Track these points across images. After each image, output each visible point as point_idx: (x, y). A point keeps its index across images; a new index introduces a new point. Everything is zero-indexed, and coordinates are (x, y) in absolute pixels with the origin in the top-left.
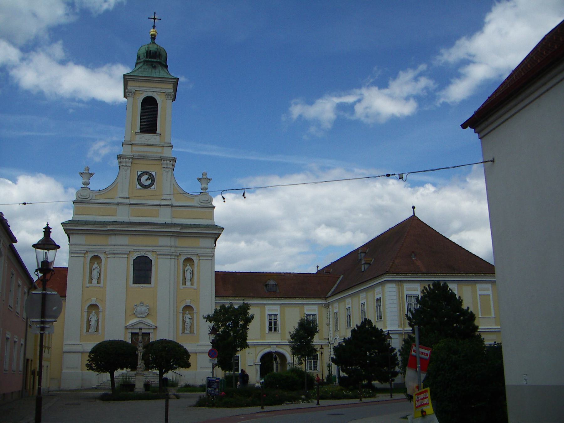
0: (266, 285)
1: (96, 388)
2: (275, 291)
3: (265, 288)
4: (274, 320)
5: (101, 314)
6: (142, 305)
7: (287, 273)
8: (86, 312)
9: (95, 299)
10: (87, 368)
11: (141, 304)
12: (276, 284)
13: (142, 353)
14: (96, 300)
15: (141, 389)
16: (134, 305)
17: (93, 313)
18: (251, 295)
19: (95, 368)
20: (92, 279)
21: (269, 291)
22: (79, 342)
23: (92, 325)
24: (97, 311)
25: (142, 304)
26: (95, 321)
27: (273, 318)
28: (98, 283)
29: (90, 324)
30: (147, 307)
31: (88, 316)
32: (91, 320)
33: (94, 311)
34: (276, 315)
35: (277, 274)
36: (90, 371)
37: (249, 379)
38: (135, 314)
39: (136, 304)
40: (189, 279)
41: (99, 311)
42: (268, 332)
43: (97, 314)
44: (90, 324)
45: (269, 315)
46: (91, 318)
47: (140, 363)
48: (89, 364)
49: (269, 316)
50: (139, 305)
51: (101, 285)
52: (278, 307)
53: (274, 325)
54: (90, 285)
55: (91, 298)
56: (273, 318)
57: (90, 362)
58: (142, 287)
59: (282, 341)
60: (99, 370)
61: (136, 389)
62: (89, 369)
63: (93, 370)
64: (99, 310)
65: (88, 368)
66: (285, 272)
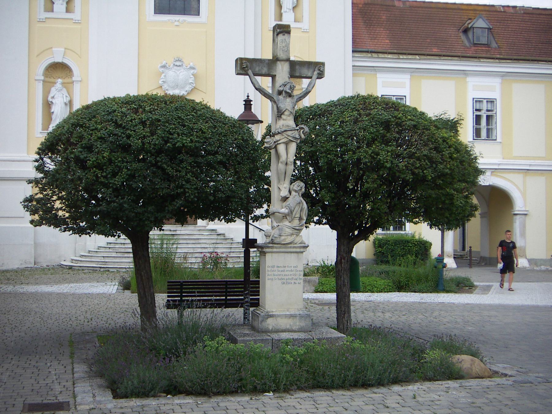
0: (466, 31)
1: (70, 268)
2: (488, 45)
3: (463, 37)
4: (488, 111)
5: (77, 88)
6: (180, 66)
7: (508, 6)
8: (42, 82)
9: (63, 49)
10: (28, 217)
11: (178, 63)
12: (491, 27)
13: (293, 147)
14: (65, 52)
15: (292, 316)
16: (160, 65)
17: (58, 85)
18: (435, 50)
19: (67, 215)
20: (53, 3)
21: (475, 45)
22: (26, 155)
23: (57, 115)
24: (67, 80)
25: (179, 63)
26: (63, 105)
27: (484, 106)
28: (68, 11)
29: (52, 111)
30: (192, 71)
31: (46, 92)
32: (54, 101)
33: (60, 81)
34: (491, 101)
35: (486, 7)
36: (44, 229)
37: (432, 249)
38: (161, 87)
39: (164, 63)
40: (291, 7)
41: (74, 79)
42: (474, 139)
43: (67, 87)
44: (52, 111)
45: (478, 101)
46: (53, 97)
47: (285, 193)
48: (38, 201)
49: (476, 101)
50: (172, 65)
51: (76, 15)
52: (405, 78)
53: (488, 123)
54: (50, 15)
55: (52, 48)
56: (484, 106)
57: (42, 190)
58: (176, 23)
59: (505, 161)
60: (83, 224)
61: (269, 316)
62: (42, 218)
63: (56, 226)
64: (72, 78)
65: (36, 217)
66: (503, 5)
